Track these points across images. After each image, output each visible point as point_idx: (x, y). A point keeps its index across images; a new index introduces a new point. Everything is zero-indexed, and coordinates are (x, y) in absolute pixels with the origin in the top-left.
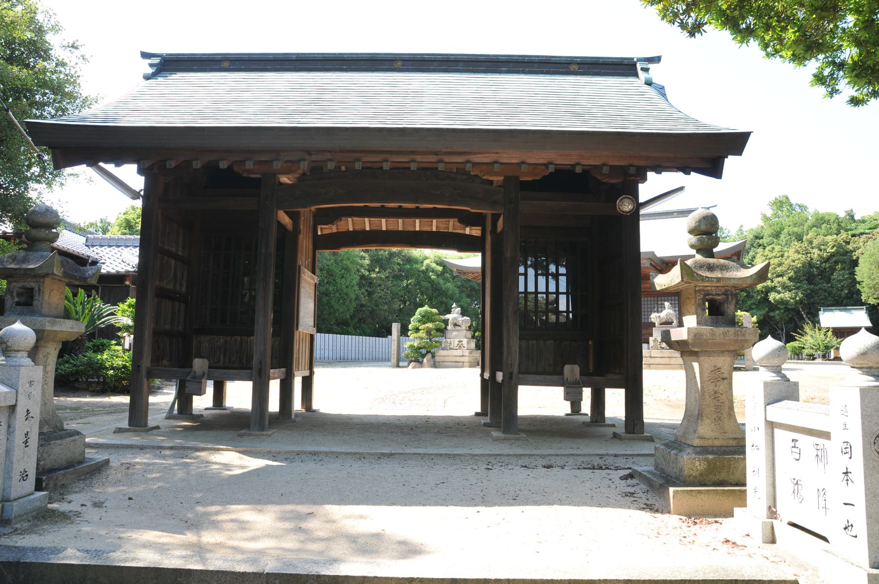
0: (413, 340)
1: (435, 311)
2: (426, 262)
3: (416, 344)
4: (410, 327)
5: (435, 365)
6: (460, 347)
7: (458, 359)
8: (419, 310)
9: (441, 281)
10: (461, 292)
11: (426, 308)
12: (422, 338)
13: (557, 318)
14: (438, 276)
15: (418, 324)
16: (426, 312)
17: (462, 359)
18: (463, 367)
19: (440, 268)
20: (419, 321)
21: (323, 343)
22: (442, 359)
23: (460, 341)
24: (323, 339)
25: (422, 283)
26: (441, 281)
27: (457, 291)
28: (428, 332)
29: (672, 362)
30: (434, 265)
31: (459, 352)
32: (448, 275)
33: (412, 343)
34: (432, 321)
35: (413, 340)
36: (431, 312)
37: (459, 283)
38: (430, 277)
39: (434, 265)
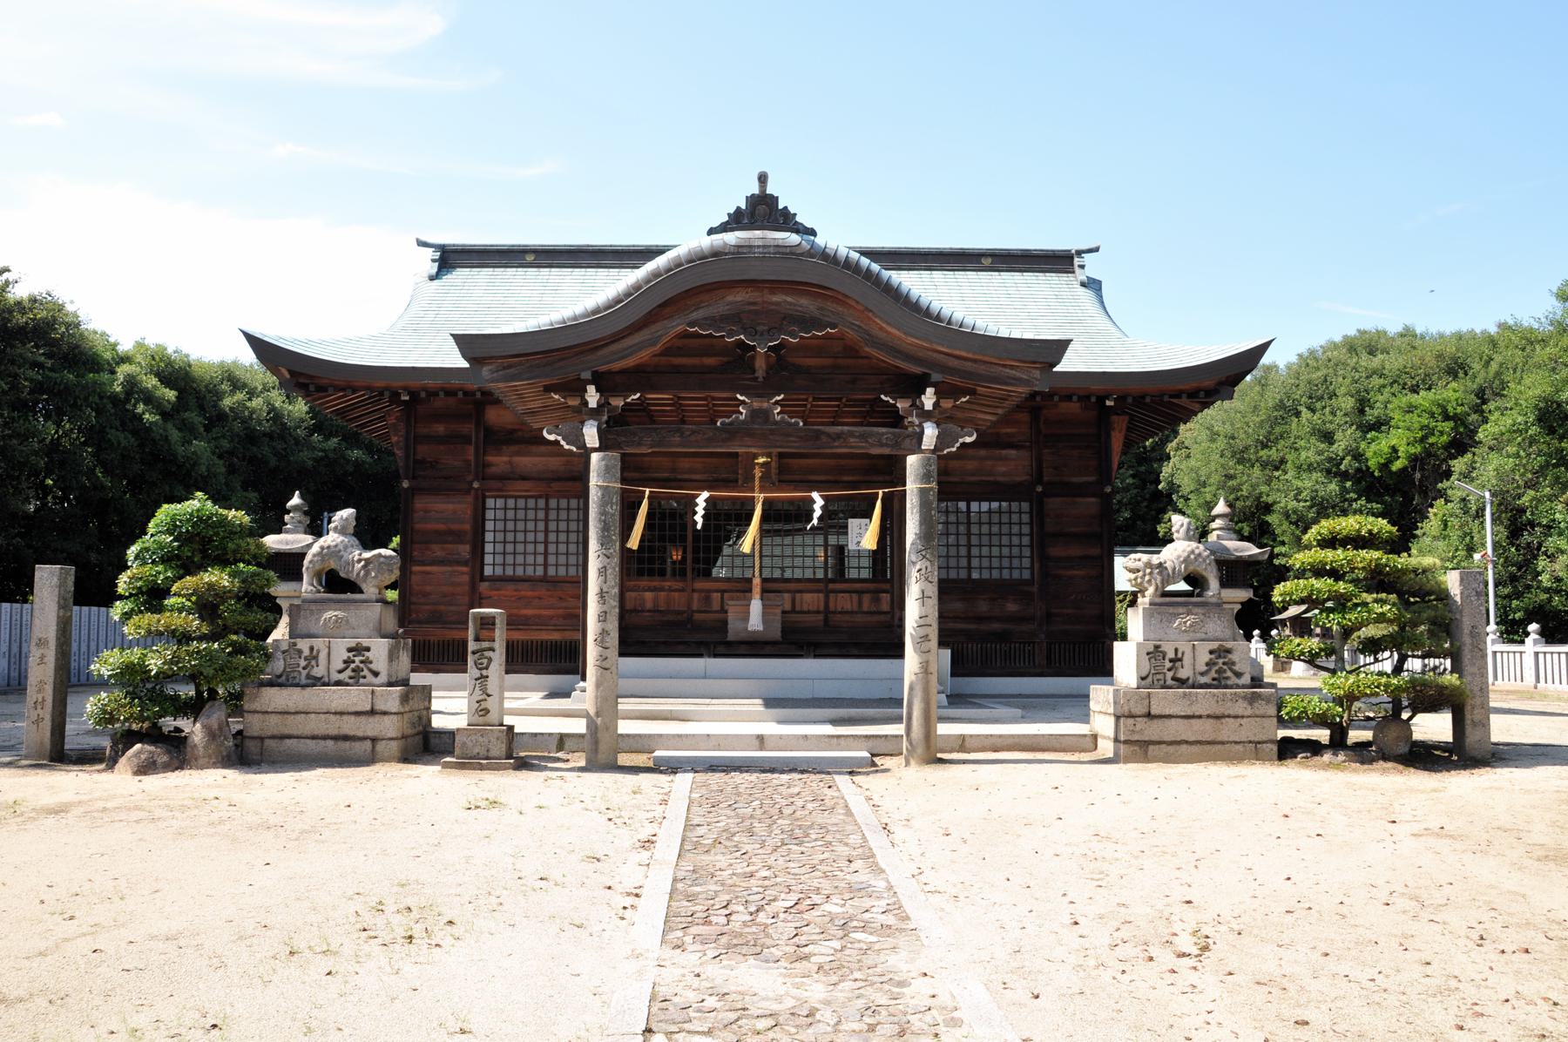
0: (128, 640)
1: (237, 516)
2: (123, 370)
3: (154, 664)
4: (123, 583)
5: (245, 753)
6: (357, 669)
7: (349, 726)
8: (165, 512)
9: (175, 435)
10: (232, 470)
11: (198, 503)
12: (184, 638)
13: (826, 540)
14: (165, 415)
15: (162, 573)
16: (201, 520)
17: (370, 727)
18: (370, 760)
19: (171, 395)
20: (166, 560)
21: (84, 632)
22: (273, 725)
23: (358, 650)
24: (85, 619)
25: (113, 435)
26: (175, 435)
27: (220, 467)
28: (207, 606)
29: (1224, 735)
30: (151, 382)
31: (355, 697)
32: (193, 417)
33: (134, 655)
34: (223, 561)
35: (128, 640)
36: (223, 522)
37: (225, 444)
38: (140, 418)
39: (151, 382)
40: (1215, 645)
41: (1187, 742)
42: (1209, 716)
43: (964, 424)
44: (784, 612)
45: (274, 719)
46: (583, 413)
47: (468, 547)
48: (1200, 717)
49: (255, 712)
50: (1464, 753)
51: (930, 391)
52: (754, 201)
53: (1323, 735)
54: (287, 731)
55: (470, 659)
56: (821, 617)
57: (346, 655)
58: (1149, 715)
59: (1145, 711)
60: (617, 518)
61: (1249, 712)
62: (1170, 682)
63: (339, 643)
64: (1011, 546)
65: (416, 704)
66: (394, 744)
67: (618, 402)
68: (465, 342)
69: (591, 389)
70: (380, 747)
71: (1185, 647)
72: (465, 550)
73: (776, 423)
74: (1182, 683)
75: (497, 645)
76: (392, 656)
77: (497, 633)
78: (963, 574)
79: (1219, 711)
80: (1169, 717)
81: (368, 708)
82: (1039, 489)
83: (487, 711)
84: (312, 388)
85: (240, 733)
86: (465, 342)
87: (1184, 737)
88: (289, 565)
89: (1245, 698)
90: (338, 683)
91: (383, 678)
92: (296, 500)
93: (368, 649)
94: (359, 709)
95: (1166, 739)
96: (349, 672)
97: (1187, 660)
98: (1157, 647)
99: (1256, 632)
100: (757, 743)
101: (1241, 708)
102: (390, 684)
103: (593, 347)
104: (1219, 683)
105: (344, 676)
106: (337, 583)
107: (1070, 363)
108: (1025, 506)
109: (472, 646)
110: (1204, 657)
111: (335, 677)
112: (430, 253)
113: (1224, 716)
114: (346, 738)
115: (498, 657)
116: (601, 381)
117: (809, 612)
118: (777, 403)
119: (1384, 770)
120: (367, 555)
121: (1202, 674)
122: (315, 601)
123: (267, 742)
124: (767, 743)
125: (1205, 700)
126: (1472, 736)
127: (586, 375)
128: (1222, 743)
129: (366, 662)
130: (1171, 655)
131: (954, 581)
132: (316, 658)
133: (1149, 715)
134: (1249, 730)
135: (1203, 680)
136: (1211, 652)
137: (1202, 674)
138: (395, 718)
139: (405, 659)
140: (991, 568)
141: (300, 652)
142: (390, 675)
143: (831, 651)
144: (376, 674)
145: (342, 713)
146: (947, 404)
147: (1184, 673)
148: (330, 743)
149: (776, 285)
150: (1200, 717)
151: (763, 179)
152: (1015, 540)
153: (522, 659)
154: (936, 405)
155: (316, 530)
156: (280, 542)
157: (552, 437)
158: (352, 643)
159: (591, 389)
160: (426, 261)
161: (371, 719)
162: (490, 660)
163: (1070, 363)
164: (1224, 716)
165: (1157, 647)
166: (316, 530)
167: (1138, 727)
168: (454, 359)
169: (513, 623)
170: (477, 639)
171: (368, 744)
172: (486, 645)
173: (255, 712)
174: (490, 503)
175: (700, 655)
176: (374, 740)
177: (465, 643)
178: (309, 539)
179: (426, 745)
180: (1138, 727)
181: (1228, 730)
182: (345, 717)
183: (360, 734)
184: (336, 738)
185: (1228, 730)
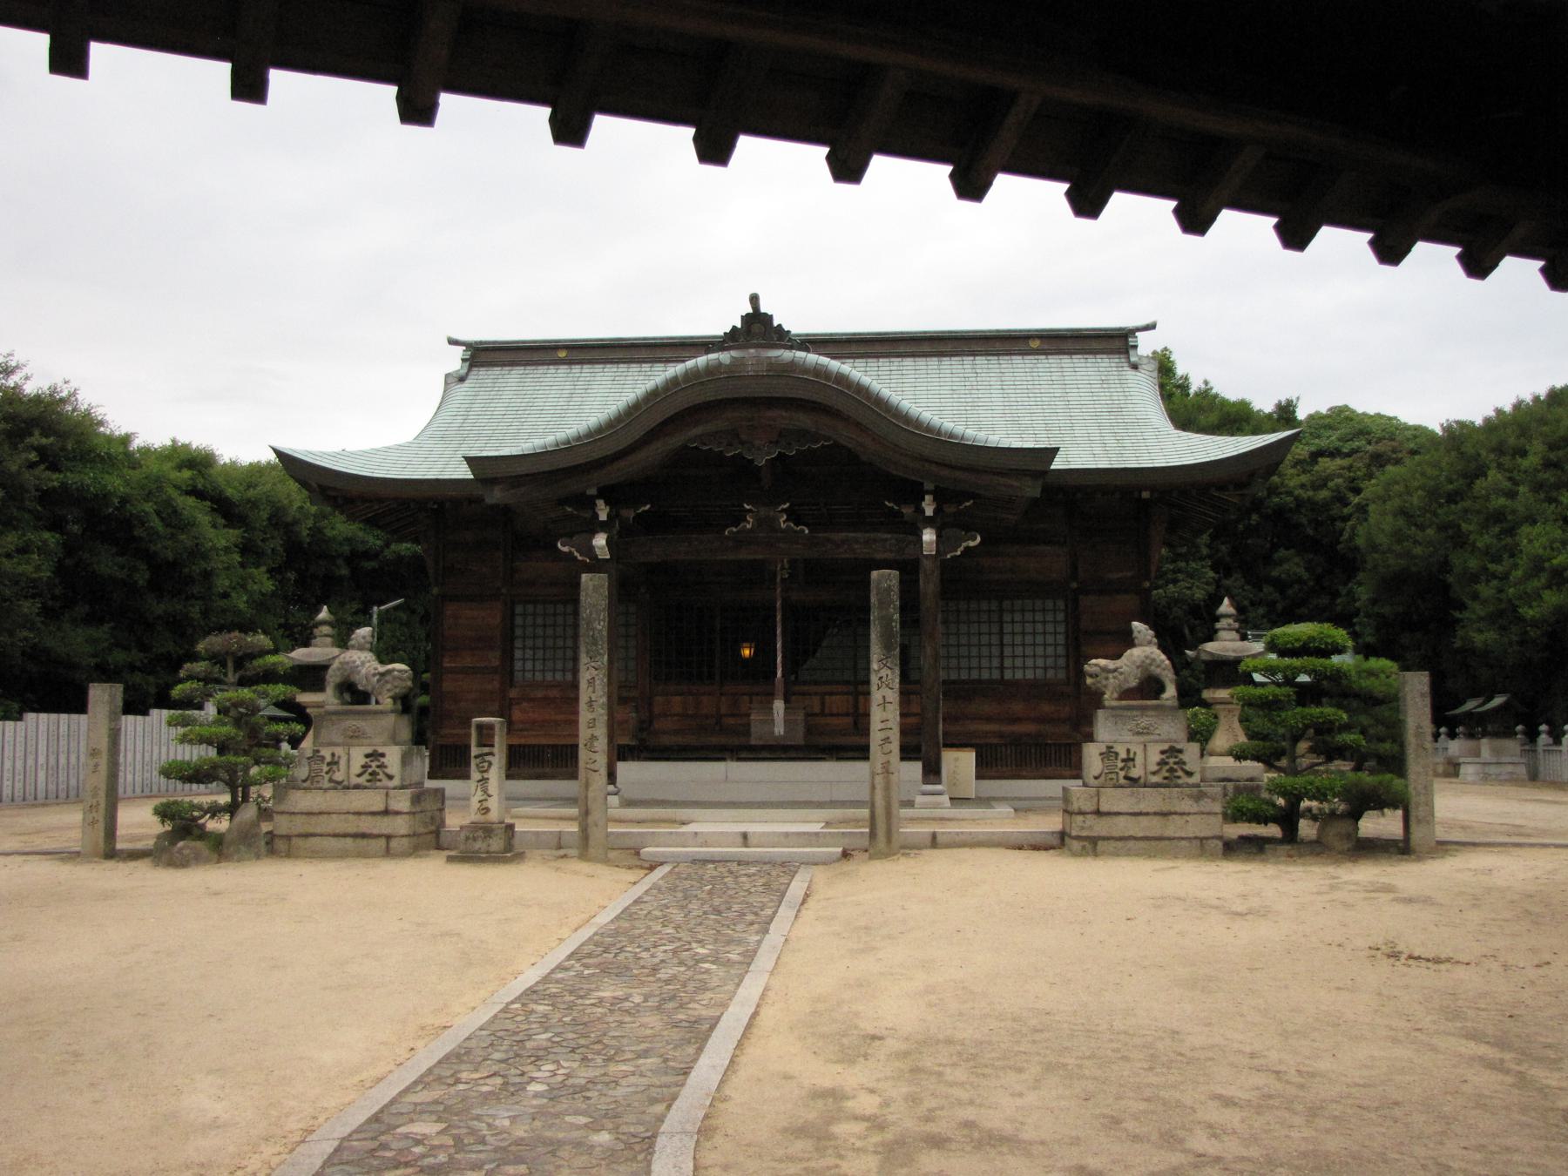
7: (366, 825)
29: (1170, 832)
31: (374, 800)
40: (1166, 747)
41: (1135, 838)
42: (1156, 814)
43: (969, 529)
44: (807, 715)
45: (299, 820)
46: (594, 527)
47: (498, 654)
48: (1147, 814)
49: (283, 813)
50: (1401, 849)
51: (928, 498)
52: (747, 319)
53: (1274, 830)
54: (311, 830)
55: (473, 763)
56: (850, 720)
57: (363, 761)
58: (1098, 813)
59: (1093, 808)
60: (605, 633)
61: (1195, 809)
62: (1122, 781)
63: (365, 754)
64: (1045, 645)
65: (429, 805)
66: (405, 841)
67: (629, 514)
68: (470, 461)
69: (600, 503)
70: (394, 844)
71: (1138, 750)
72: (494, 658)
73: (783, 531)
74: (1133, 782)
75: (496, 750)
76: (405, 760)
77: (497, 739)
78: (996, 675)
79: (1165, 809)
80: (1118, 814)
81: (381, 807)
82: (1074, 585)
83: (487, 810)
84: (340, 501)
85: (270, 833)
86: (470, 461)
87: (1131, 833)
88: (312, 676)
89: (1190, 796)
90: (357, 787)
91: (396, 782)
92: (324, 614)
93: (383, 755)
94: (374, 809)
95: (1115, 834)
96: (366, 776)
97: (1139, 760)
98: (1109, 748)
99: (1543, 727)
100: (740, 839)
101: (1187, 805)
102: (402, 787)
103: (600, 464)
104: (1170, 782)
105: (362, 780)
106: (353, 693)
107: (1058, 464)
108: (1061, 604)
109: (474, 751)
110: (1155, 757)
111: (355, 780)
112: (459, 351)
113: (1170, 813)
114: (364, 836)
115: (498, 760)
116: (607, 493)
117: (838, 715)
118: (783, 511)
119: (1277, 863)
120: (382, 669)
121: (1154, 773)
122: (336, 713)
123: (294, 840)
124: (752, 840)
125: (1151, 800)
126: (1417, 834)
127: (592, 491)
128: (1169, 839)
129: (382, 766)
130: (1123, 755)
131: (954, 682)
132: (337, 763)
133: (1098, 813)
134: (1196, 827)
135: (1155, 779)
136: (1163, 752)
137: (1154, 773)
138: (406, 817)
139: (422, 764)
140: (1024, 668)
141: (323, 758)
142: (402, 779)
143: (850, 754)
144: (390, 777)
145: (359, 814)
146: (950, 509)
147: (1136, 772)
148: (349, 841)
149: (771, 402)
150: (1147, 814)
151: (754, 299)
152: (1050, 639)
153: (522, 762)
154: (935, 511)
155: (343, 642)
156: (309, 655)
157: (566, 549)
158: (369, 750)
159: (600, 503)
160: (454, 360)
161: (386, 819)
162: (490, 764)
163: (1058, 464)
164: (1170, 813)
165: (1109, 748)
166: (343, 642)
167: (1088, 823)
168: (464, 472)
169: (510, 727)
170: (481, 744)
171: (383, 842)
172: (486, 750)
173: (283, 813)
174: (519, 609)
175: (723, 759)
176: (389, 837)
177: (468, 747)
178: (336, 651)
179: (431, 838)
180: (1088, 823)
181: (1173, 827)
182: (363, 817)
183: (375, 831)
184: (355, 836)
185: (1173, 827)
